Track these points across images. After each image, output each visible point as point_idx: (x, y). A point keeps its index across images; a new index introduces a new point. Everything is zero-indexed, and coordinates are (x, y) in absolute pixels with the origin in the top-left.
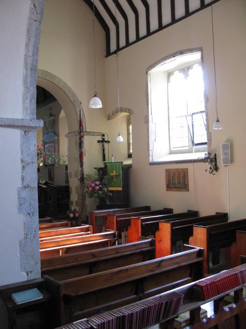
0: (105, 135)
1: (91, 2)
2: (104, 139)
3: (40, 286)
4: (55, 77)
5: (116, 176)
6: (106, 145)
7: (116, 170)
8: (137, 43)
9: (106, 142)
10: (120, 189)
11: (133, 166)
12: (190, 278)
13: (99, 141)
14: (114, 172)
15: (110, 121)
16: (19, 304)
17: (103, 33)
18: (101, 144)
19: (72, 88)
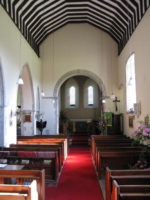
0: (118, 98)
1: (126, 1)
2: (116, 100)
3: (52, 159)
4: (89, 72)
5: (109, 119)
6: (118, 103)
7: (109, 116)
8: (7, 14)
9: (117, 101)
10: (111, 125)
11: (124, 114)
12: (50, 176)
13: (114, 101)
14: (109, 117)
15: (120, 90)
16: (23, 163)
17: (87, 24)
18: (115, 102)
19: (98, 76)
